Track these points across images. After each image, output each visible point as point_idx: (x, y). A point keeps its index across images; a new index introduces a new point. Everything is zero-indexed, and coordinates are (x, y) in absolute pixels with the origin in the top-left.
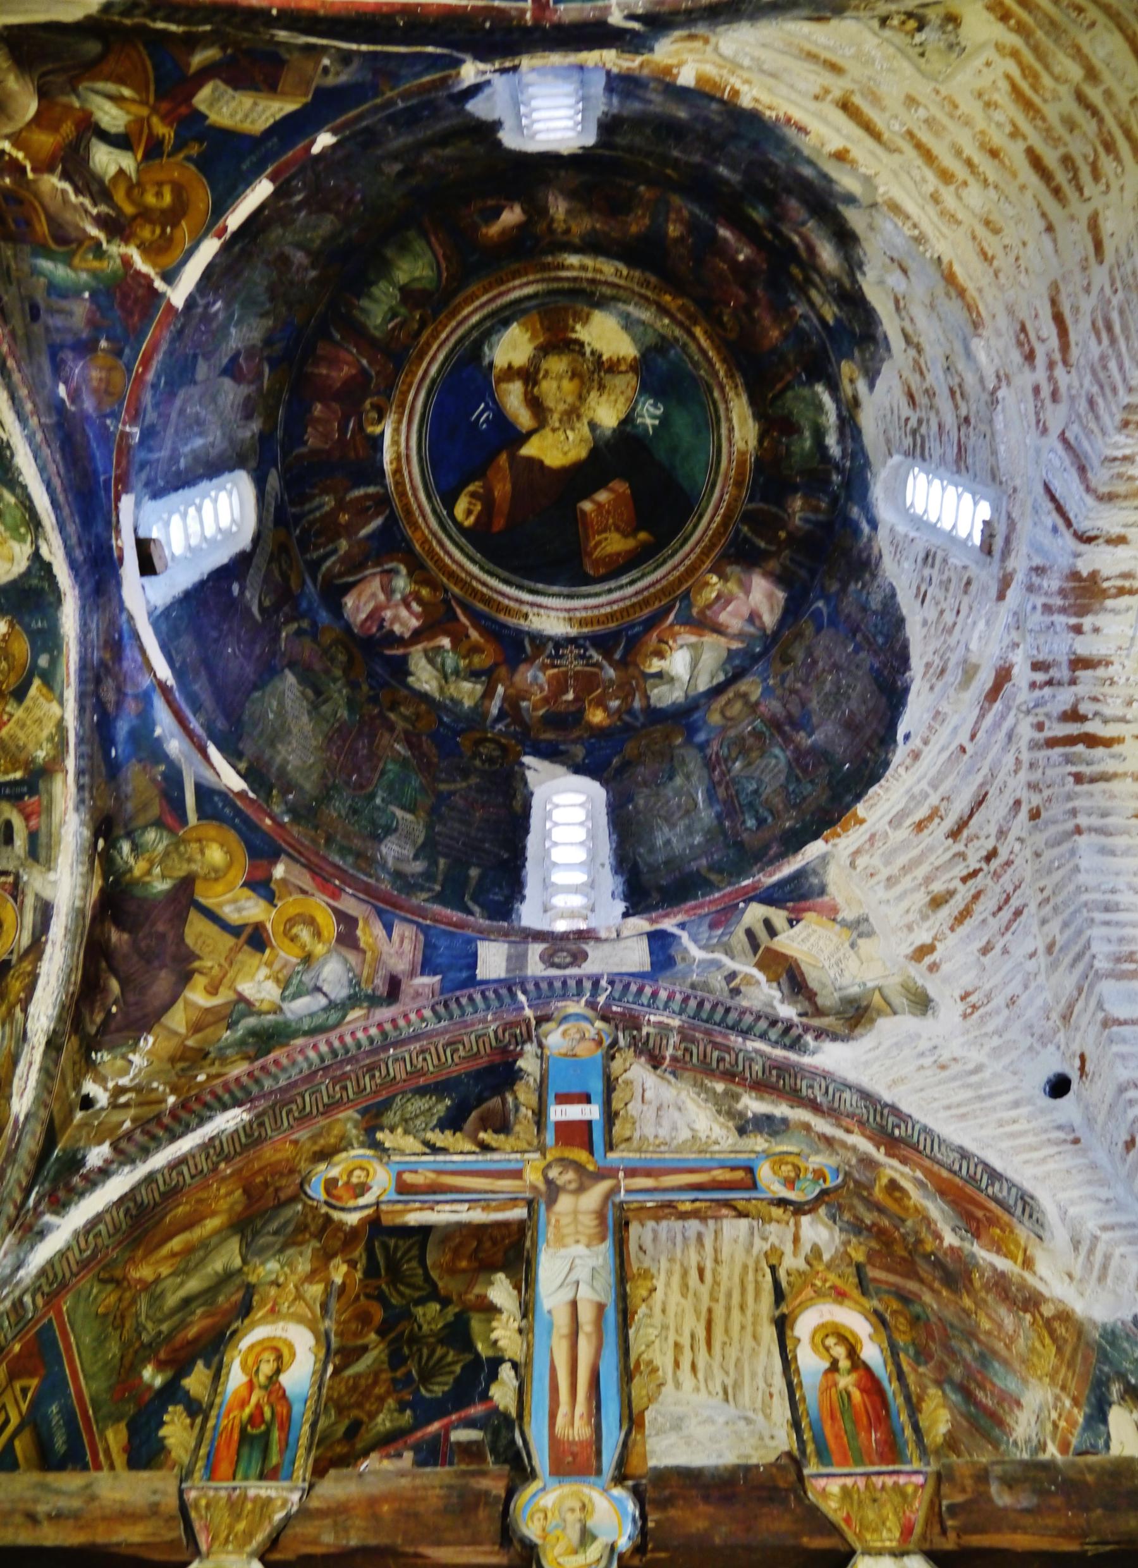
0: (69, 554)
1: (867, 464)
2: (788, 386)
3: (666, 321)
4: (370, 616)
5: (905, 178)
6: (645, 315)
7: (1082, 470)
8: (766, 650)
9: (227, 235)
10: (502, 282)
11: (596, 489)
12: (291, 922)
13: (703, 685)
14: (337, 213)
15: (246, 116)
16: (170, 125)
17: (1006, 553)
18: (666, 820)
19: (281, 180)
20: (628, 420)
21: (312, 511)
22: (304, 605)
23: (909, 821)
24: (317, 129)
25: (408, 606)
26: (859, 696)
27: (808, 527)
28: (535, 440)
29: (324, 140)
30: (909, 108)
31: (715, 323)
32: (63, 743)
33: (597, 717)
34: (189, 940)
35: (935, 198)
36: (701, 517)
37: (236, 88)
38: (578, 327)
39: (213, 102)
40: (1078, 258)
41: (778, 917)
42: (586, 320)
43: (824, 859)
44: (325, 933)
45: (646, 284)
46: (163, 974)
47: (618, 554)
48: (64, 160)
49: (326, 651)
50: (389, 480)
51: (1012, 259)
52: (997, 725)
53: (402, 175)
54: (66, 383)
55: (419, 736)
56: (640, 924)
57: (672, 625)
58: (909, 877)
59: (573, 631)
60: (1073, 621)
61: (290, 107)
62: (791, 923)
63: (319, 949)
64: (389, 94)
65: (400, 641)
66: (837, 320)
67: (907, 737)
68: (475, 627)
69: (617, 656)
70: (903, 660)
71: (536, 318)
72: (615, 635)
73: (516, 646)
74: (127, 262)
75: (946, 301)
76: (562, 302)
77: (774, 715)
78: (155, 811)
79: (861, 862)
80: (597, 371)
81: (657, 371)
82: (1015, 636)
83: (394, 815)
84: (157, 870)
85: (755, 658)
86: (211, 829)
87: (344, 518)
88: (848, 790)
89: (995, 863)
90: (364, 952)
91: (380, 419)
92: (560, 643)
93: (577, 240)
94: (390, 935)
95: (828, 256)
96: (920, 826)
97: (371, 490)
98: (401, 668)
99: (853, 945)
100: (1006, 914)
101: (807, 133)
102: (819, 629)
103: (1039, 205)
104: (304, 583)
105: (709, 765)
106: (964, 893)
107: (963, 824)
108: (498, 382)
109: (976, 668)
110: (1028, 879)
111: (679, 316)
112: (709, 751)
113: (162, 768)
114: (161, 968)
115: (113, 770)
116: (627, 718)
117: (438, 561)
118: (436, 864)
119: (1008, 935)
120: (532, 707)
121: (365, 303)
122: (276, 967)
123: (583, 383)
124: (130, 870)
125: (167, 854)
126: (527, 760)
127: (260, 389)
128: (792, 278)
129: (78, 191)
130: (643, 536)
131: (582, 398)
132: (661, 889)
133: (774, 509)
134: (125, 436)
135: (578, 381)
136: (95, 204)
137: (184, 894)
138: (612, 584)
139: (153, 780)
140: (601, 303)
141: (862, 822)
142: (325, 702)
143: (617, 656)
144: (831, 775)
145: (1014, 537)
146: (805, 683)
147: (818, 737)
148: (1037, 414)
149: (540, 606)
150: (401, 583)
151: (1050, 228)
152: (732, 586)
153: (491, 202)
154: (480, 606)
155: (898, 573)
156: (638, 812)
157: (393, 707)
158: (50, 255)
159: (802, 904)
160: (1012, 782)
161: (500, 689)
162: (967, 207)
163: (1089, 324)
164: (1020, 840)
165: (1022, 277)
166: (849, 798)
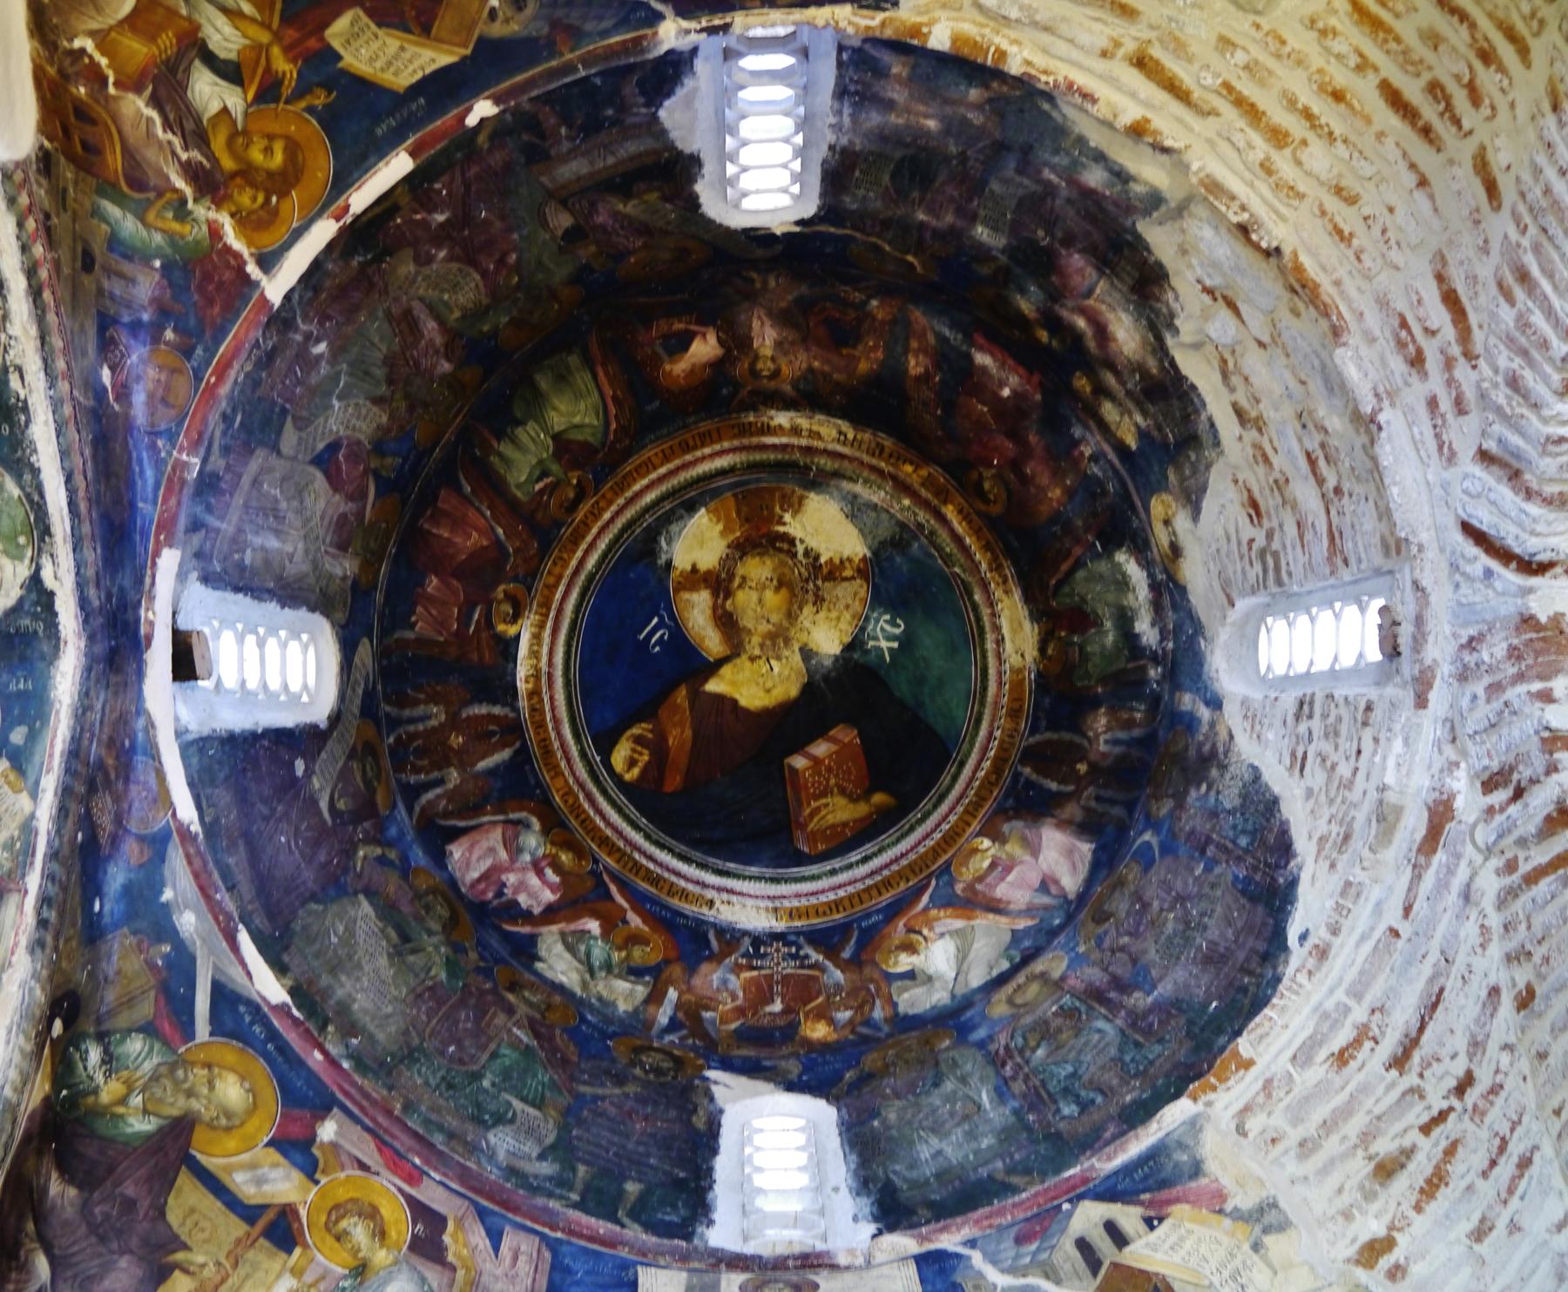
0: (80, 586)
1: (1199, 628)
2: (1079, 564)
3: (907, 502)
4: (485, 877)
5: (1224, 147)
6: (877, 496)
7: (1514, 476)
8: (1070, 918)
9: (348, 219)
10: (688, 449)
11: (811, 739)
12: (339, 1210)
13: (976, 978)
14: (484, 274)
15: (389, 64)
16: (294, 61)
17: (1419, 641)
18: (934, 1131)
19: (425, 156)
20: (855, 645)
21: (412, 720)
22: (393, 832)
23: (1323, 1054)
24: (476, 93)
25: (540, 873)
26: (1220, 921)
27: (1118, 750)
28: (726, 670)
29: (483, 109)
30: (1222, 53)
31: (974, 491)
32: (29, 850)
33: (819, 1031)
34: (173, 1217)
35: (1267, 168)
36: (962, 764)
37: (380, 25)
38: (787, 517)
39: (351, 37)
40: (1466, 212)
41: (1128, 1217)
42: (797, 507)
43: (1194, 1125)
44: (393, 1234)
45: (878, 451)
46: (124, 1262)
47: (845, 825)
48: (156, 81)
49: (418, 896)
50: (523, 703)
51: (1376, 231)
52: (1442, 885)
53: (574, 235)
54: (112, 369)
55: (551, 1027)
56: (904, 1243)
57: (926, 909)
58: (1334, 1139)
59: (780, 926)
60: (1536, 686)
61: (445, 59)
62: (1150, 1223)
63: (381, 1257)
64: (569, 56)
65: (527, 916)
66: (1142, 434)
67: (1303, 937)
68: (634, 909)
69: (846, 954)
70: (1284, 848)
71: (731, 503)
72: (844, 929)
73: (695, 941)
74: (215, 232)
75: (1294, 322)
76: (766, 481)
77: (1091, 984)
78: (146, 1009)
79: (1254, 1124)
80: (810, 579)
81: (898, 576)
82: (1450, 752)
83: (509, 1104)
84: (137, 1100)
85: (1053, 933)
86: (229, 1052)
87: (457, 740)
88: (1220, 1031)
89: (1472, 1096)
90: (453, 1269)
91: (515, 617)
92: (759, 940)
93: (787, 388)
94: (496, 1249)
95: (1126, 334)
96: (1342, 1058)
97: (497, 710)
98: (526, 950)
99: (1256, 1247)
100: (1506, 1168)
101: (1094, 101)
102: (1148, 865)
103: (1405, 154)
104: (394, 806)
105: (996, 1061)
106: (1428, 1151)
107: (1411, 1044)
108: (676, 591)
109: (1399, 811)
110: (1532, 1105)
111: (923, 492)
112: (992, 1047)
113: (166, 948)
114: (122, 1253)
115: (94, 933)
116: (864, 1030)
117: (586, 821)
118: (574, 1170)
119: (1515, 1202)
120: (721, 1017)
121: (506, 448)
122: (309, 1277)
123: (793, 595)
124: (96, 1091)
125: (155, 1078)
126: (712, 1074)
127: (360, 514)
128: (1075, 395)
129: (167, 125)
130: (879, 798)
131: (791, 616)
132: (931, 1205)
133: (1066, 736)
134: (181, 466)
135: (785, 591)
136: (186, 148)
137: (174, 1148)
138: (837, 863)
139: (151, 965)
140: (817, 481)
141: (1248, 1064)
142: (414, 951)
143: (846, 954)
144: (1191, 1023)
145: (1428, 614)
146: (1134, 934)
147: (1165, 989)
148: (1437, 436)
149: (731, 891)
150: (532, 841)
151: (1423, 183)
152: (1013, 848)
153: (679, 326)
154: (644, 886)
155: (1258, 750)
156: (888, 1128)
157: (513, 987)
158: (120, 200)
159: (1164, 1194)
160: (1480, 963)
161: (672, 994)
162: (1308, 174)
163: (1494, 290)
164: (1507, 1047)
165: (1395, 255)
166: (1222, 1040)
